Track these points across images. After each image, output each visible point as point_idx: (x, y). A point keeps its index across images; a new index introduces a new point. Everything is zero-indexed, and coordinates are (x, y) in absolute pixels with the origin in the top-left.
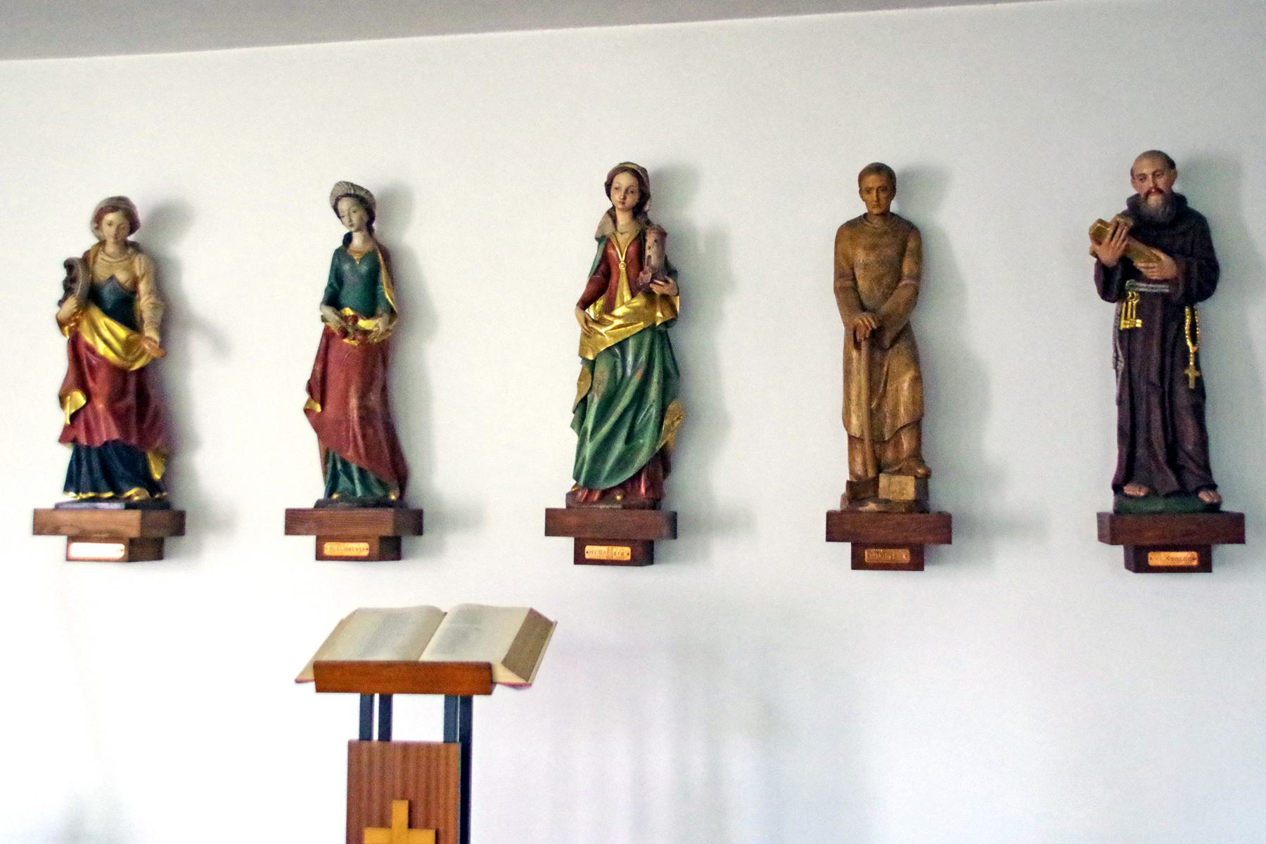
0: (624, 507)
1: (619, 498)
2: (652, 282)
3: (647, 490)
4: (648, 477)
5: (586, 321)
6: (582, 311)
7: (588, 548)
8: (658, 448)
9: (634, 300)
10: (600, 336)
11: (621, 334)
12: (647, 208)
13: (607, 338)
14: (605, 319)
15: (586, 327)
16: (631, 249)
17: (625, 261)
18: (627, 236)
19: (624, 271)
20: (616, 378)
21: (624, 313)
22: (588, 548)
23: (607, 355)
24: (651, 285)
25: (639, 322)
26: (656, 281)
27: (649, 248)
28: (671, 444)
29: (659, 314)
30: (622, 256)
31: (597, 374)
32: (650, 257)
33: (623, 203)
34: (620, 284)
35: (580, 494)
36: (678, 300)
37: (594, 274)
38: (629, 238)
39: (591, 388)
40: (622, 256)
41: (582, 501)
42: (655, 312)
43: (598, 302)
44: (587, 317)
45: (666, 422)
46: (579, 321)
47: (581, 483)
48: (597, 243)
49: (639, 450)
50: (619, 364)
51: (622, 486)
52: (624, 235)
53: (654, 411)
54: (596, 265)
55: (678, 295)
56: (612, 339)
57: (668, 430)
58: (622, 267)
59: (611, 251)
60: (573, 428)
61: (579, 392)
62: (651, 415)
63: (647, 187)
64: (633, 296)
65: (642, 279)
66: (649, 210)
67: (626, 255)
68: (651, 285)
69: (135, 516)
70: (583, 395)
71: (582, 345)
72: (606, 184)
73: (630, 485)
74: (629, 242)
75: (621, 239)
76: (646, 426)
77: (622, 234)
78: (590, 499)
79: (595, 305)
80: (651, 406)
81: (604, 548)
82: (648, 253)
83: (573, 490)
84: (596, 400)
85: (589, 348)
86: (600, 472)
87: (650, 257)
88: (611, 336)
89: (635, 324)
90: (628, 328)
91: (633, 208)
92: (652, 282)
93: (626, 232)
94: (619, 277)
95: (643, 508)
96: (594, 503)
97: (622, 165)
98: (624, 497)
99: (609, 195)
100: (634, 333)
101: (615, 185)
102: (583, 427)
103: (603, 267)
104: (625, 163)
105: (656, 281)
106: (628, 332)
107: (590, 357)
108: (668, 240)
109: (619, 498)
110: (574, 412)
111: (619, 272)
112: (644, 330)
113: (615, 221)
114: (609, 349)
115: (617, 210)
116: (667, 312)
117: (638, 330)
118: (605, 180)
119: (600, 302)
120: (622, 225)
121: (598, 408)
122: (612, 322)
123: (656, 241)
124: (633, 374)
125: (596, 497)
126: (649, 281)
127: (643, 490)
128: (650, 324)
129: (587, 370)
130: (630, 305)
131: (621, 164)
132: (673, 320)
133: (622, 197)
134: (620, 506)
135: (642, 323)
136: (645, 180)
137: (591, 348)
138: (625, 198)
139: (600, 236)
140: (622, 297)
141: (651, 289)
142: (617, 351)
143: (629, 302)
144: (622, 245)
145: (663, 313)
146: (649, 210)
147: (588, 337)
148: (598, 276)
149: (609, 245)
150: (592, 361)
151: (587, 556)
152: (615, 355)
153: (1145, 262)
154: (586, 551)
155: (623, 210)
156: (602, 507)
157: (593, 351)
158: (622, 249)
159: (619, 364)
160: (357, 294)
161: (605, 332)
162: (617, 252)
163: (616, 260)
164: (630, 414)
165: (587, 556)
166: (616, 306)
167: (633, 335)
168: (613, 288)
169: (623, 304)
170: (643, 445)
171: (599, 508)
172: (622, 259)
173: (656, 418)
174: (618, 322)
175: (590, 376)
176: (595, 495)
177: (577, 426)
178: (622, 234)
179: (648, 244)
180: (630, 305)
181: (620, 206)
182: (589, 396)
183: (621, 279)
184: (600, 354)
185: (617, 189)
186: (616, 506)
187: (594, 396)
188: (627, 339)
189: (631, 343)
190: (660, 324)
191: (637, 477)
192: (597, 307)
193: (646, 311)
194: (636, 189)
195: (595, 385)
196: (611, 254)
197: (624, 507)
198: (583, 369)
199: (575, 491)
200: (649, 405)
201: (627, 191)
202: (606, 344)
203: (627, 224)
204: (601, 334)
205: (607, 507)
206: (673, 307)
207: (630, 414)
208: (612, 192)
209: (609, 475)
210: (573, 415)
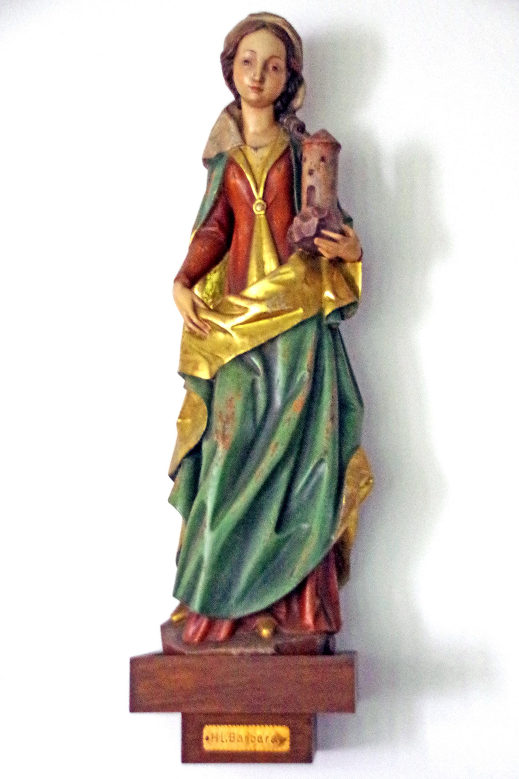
0: (279, 651)
1: (265, 632)
2: (318, 234)
3: (316, 617)
4: (317, 594)
5: (195, 308)
6: (187, 291)
7: (208, 730)
8: (335, 538)
9: (285, 269)
10: (220, 336)
11: (264, 330)
12: (297, 102)
13: (237, 340)
14: (231, 304)
15: (195, 320)
16: (276, 176)
17: (264, 198)
18: (264, 152)
19: (263, 216)
20: (254, 410)
21: (266, 293)
22: (208, 730)
23: (240, 369)
24: (316, 241)
25: (296, 308)
26: (324, 232)
27: (311, 173)
28: (352, 531)
29: (328, 294)
30: (257, 189)
31: (218, 403)
32: (311, 188)
33: (259, 90)
34: (255, 242)
35: (191, 629)
36: (360, 270)
37: (204, 225)
38: (270, 156)
39: (206, 434)
40: (257, 189)
41: (196, 640)
42: (321, 291)
43: (209, 277)
44: (197, 301)
45: (347, 490)
46: (181, 308)
47: (196, 606)
48: (204, 172)
49: (301, 543)
50: (260, 386)
51: (270, 611)
52: (260, 151)
53: (325, 469)
54: (208, 207)
55: (359, 260)
56: (246, 340)
57: (351, 506)
58: (258, 210)
59: (236, 181)
60: (175, 505)
61: (182, 438)
62: (320, 478)
63: (299, 60)
64: (281, 262)
65: (299, 230)
66: (300, 107)
67: (265, 188)
68: (316, 241)
69: (351, 231)
70: (192, 443)
71: (185, 351)
72: (223, 55)
73: (283, 609)
74: (271, 162)
75: (254, 158)
76: (312, 496)
77: (256, 149)
78: (211, 637)
79: (205, 283)
80: (321, 461)
81: (241, 730)
82: (307, 181)
83: (175, 618)
84: (221, 452)
85: (200, 358)
86: (230, 584)
87: (311, 188)
88: (243, 334)
89: (290, 311)
90: (275, 319)
91: (275, 103)
92: (318, 234)
93: (266, 146)
94: (252, 231)
95: (312, 653)
96: (218, 644)
97: (255, 18)
98: (275, 632)
99: (229, 79)
100: (286, 329)
101: (243, 53)
102: (196, 503)
103: (219, 212)
104: (259, 15)
105: (324, 232)
106: (277, 325)
107: (204, 373)
108: (342, 155)
109: (265, 632)
110: (173, 476)
111: (252, 218)
112: (302, 323)
113: (240, 126)
114: (240, 359)
115: (244, 105)
116: (343, 291)
117: (295, 322)
118: (220, 48)
119: (213, 277)
120: (255, 134)
121: (225, 466)
122: (246, 309)
123: (323, 159)
124: (286, 403)
125: (223, 632)
126: (312, 234)
127: (309, 619)
128: (313, 312)
129: (197, 398)
130: (278, 278)
131: (252, 15)
132: (354, 304)
133: (257, 78)
134: (270, 650)
135: (300, 311)
136: (297, 46)
137: (204, 357)
138: (262, 80)
139: (213, 153)
140: (261, 264)
141: (316, 247)
142: (256, 361)
143: (273, 274)
144: (257, 170)
145: (335, 293)
146: (300, 107)
147: (201, 338)
148: (211, 229)
149: (232, 170)
150: (208, 381)
151: (207, 746)
152: (252, 369)
153: (337, 331)
154: (204, 736)
155: (257, 105)
156: (234, 651)
157: (210, 364)
158: (257, 176)
159: (260, 386)
160: (328, 531)
161: (233, 328)
162: (248, 183)
163: (247, 197)
164: (284, 476)
165: (207, 746)
166: (250, 283)
167: (284, 333)
168: (242, 249)
169: (262, 276)
170: (309, 533)
171: (231, 655)
172: (258, 195)
173: (330, 484)
174: (256, 309)
175: (205, 407)
176: (219, 631)
177: (181, 502)
178: (256, 149)
179: (306, 167)
180: (278, 278)
181: (253, 96)
182: (206, 446)
183: (256, 228)
184: (223, 368)
185: (246, 62)
186: (261, 650)
187: (216, 446)
188: (272, 341)
189: (281, 346)
190: (333, 312)
191: (300, 590)
192: (209, 286)
193: (306, 288)
194: (282, 63)
195: (217, 425)
196: (235, 186)
197: (279, 651)
198: (188, 395)
199: (180, 621)
200: (315, 461)
201: (265, 67)
202: (235, 350)
203: (264, 132)
204: (225, 332)
205: (248, 650)
206: (350, 282)
207: (284, 476)
208: (237, 67)
209: (244, 593)
210: (171, 483)
